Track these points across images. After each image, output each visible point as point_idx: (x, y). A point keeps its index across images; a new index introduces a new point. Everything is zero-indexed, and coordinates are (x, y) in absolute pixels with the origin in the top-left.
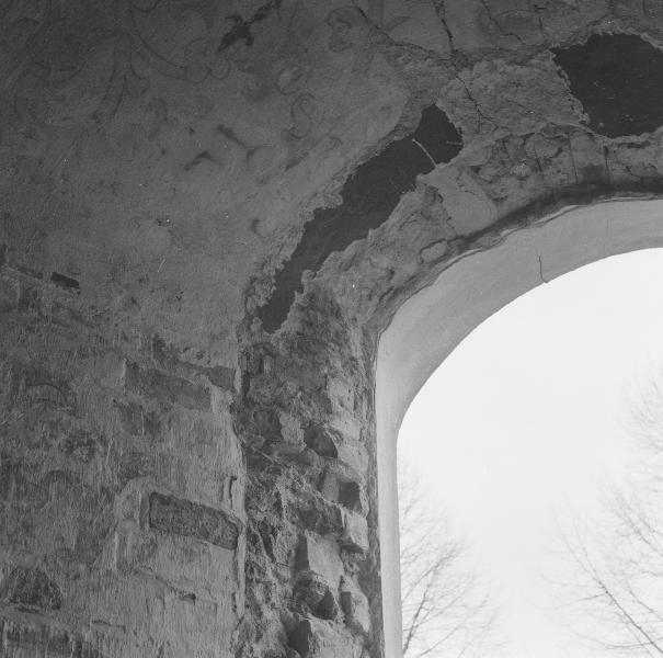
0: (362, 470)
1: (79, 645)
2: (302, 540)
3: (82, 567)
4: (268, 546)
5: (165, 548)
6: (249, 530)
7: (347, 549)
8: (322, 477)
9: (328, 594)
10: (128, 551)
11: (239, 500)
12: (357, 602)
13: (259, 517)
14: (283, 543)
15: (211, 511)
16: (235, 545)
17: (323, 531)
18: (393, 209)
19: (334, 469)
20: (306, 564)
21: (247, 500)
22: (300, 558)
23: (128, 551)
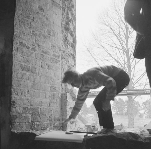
0: (74, 3)
1: (46, 17)
2: (68, 11)
3: (45, 7)
4: (64, 10)
5: (54, 7)
6: (62, 8)
7: (72, 14)
8: (70, 3)
9: (70, 19)
10: (50, 7)
11: (61, 3)
12: (71, 108)
13: (63, 6)
14: (66, 10)
15: (57, 4)
16: (61, 9)
17: (70, 11)
18: (93, 138)
19: (72, 2)
20: (68, 15)
21: (62, 4)
22: (67, 14)
23: (50, 7)
